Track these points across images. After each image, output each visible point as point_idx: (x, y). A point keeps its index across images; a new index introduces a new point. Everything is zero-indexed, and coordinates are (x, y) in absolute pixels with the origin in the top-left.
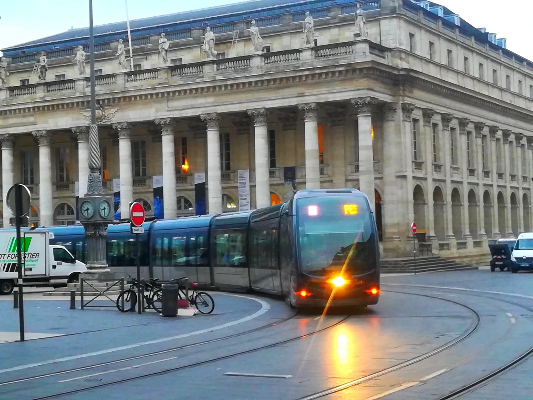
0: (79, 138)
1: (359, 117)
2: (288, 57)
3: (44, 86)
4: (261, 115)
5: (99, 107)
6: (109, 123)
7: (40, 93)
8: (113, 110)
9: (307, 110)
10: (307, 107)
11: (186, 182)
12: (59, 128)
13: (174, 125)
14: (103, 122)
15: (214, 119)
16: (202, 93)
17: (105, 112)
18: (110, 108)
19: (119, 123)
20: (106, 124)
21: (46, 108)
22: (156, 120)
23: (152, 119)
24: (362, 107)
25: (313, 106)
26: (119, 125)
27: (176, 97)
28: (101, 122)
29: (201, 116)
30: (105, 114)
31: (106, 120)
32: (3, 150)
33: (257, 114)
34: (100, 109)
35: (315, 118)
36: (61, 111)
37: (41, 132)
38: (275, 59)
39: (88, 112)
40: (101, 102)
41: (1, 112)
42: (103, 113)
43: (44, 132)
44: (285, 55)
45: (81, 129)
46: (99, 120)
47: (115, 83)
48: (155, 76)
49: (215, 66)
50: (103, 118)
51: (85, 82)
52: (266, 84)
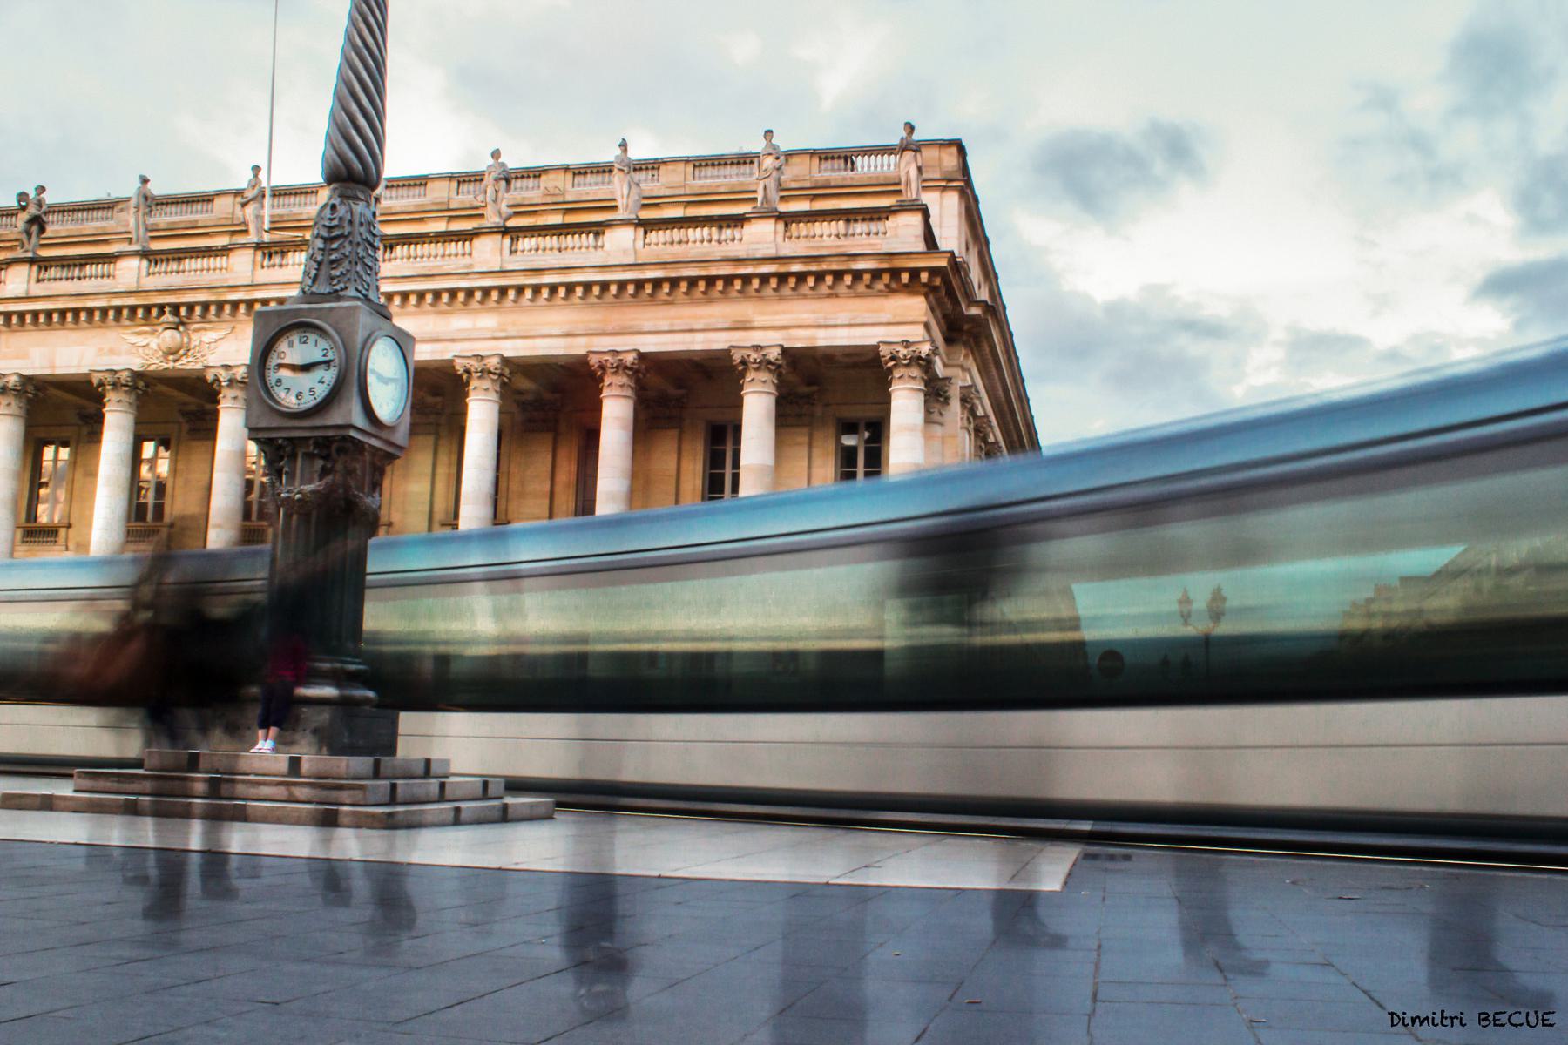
0: (109, 401)
1: (746, 393)
2: (710, 234)
3: (141, 260)
4: (626, 368)
5: (174, 323)
6: (199, 366)
7: (621, 244)
8: (209, 336)
9: (755, 363)
10: (756, 356)
11: (56, 541)
12: (58, 371)
13: (140, 392)
14: (180, 362)
15: (492, 369)
16: (465, 303)
17: (190, 338)
18: (205, 329)
19: (227, 367)
20: (188, 367)
21: (28, 318)
22: (591, 356)
23: (85, 370)
24: (907, 366)
25: (630, 358)
26: (906, 347)
27: (625, 300)
28: (175, 361)
29: (458, 361)
30: (189, 343)
31: (190, 359)
32: (606, 397)
33: (615, 365)
34: (177, 329)
35: (494, 394)
36: (100, 327)
37: (5, 380)
38: (221, 264)
39: (144, 336)
40: (183, 311)
41: (8, 316)
42: (186, 340)
43: (126, 374)
44: (409, 247)
45: (119, 378)
46: (171, 357)
47: (226, 269)
48: (685, 239)
49: (507, 241)
50: (182, 352)
51: (145, 263)
52: (849, 283)
